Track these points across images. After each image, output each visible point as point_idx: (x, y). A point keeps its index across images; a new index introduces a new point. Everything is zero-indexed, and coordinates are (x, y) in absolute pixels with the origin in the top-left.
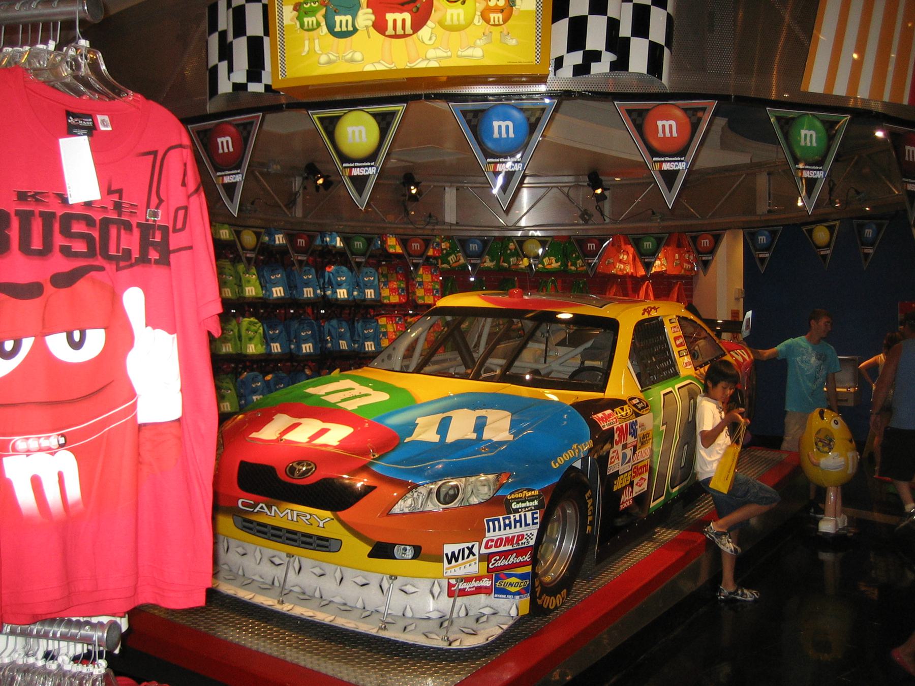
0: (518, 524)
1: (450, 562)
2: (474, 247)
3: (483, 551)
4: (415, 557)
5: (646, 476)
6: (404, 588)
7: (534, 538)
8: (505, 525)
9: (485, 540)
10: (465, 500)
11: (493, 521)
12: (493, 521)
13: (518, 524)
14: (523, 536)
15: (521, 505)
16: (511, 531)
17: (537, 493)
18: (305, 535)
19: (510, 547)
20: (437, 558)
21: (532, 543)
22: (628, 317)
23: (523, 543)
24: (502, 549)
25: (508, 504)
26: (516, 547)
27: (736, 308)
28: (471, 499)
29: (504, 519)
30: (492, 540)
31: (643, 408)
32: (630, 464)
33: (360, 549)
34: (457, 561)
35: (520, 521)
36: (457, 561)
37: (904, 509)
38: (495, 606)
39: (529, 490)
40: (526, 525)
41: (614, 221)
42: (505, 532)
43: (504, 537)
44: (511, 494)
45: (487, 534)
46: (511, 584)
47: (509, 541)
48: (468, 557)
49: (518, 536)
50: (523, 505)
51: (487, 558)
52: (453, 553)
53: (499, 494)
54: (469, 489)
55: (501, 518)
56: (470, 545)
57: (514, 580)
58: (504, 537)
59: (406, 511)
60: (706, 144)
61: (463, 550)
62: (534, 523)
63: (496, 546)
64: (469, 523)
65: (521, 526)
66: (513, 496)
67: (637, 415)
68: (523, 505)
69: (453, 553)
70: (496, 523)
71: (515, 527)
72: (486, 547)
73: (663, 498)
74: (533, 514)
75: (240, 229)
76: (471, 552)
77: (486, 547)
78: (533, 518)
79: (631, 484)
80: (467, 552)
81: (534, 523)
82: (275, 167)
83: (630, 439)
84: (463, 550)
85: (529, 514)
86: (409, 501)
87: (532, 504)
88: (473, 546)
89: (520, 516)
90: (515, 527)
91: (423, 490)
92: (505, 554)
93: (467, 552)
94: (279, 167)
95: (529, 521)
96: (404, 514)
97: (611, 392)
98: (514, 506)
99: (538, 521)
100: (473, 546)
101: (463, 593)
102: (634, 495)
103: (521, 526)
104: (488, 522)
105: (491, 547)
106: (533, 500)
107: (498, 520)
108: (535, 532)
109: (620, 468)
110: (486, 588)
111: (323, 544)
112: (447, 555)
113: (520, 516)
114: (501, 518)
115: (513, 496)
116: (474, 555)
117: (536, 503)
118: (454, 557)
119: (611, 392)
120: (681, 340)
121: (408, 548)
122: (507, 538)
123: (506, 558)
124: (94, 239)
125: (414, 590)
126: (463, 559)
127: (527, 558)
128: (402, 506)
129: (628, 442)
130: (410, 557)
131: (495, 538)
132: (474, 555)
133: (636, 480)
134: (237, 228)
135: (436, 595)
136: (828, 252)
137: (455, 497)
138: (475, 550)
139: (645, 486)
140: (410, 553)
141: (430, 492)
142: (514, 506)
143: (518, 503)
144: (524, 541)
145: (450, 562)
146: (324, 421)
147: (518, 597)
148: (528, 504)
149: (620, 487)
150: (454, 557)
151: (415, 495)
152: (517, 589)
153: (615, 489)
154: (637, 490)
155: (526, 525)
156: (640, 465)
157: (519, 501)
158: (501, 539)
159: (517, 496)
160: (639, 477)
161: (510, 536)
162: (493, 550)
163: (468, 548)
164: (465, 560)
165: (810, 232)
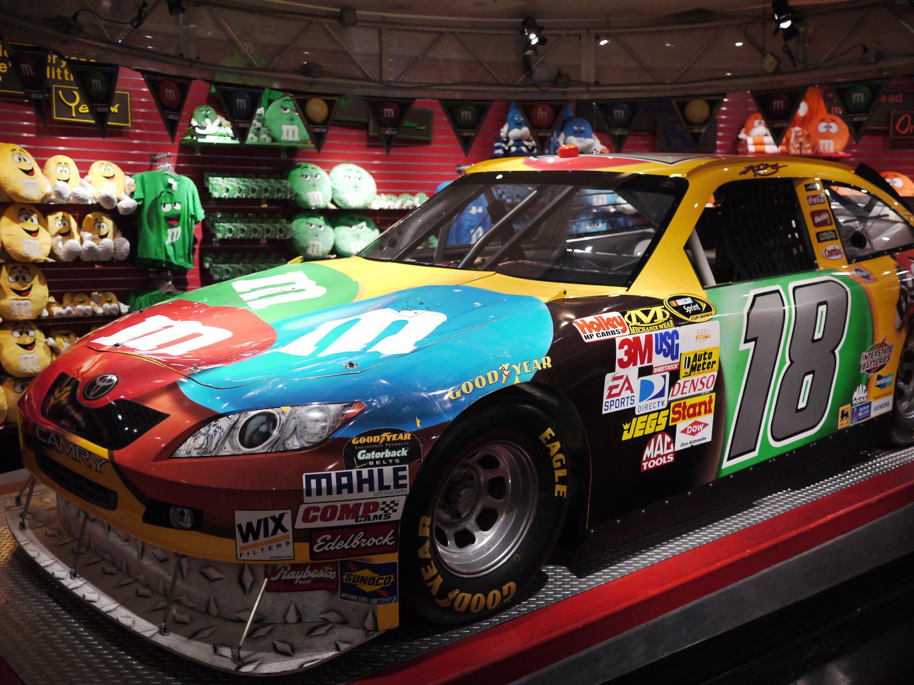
0: (366, 486)
1: (245, 539)
2: (619, 113)
3: (300, 524)
5: (709, 419)
6: (205, 571)
9: (302, 508)
11: (318, 479)
12: (318, 479)
13: (366, 486)
14: (376, 505)
16: (351, 496)
17: (408, 436)
19: (351, 522)
21: (396, 516)
24: (335, 523)
28: (289, 442)
29: (339, 477)
30: (316, 509)
32: (665, 399)
35: (370, 480)
36: (256, 537)
37: (417, 554)
39: (393, 431)
42: (340, 497)
43: (339, 505)
44: (359, 437)
45: (306, 499)
46: (364, 580)
47: (348, 511)
49: (367, 505)
50: (379, 455)
52: (250, 525)
53: (339, 435)
56: (277, 513)
57: (366, 573)
58: (339, 505)
59: (194, 454)
62: (397, 486)
63: (324, 518)
65: (371, 489)
66: (363, 440)
67: (677, 322)
68: (379, 455)
69: (250, 525)
71: (360, 490)
73: (754, 454)
74: (396, 471)
77: (305, 519)
78: (397, 478)
79: (670, 431)
80: (272, 525)
81: (397, 486)
83: (659, 360)
84: (266, 520)
85: (388, 471)
86: (201, 440)
87: (394, 454)
92: (345, 532)
98: (361, 455)
99: (407, 482)
100: (282, 516)
101: (288, 586)
102: (678, 447)
104: (309, 479)
105: (315, 519)
106: (397, 448)
107: (328, 477)
108: (402, 501)
110: (328, 581)
112: (240, 526)
115: (363, 440)
116: (284, 530)
118: (251, 532)
121: (186, 512)
122: (345, 508)
124: (71, 102)
125: (219, 575)
126: (266, 535)
131: (322, 506)
132: (284, 530)
133: (681, 425)
134: (300, 97)
138: (287, 522)
139: (706, 435)
140: (188, 522)
141: (233, 427)
142: (361, 455)
143: (369, 451)
144: (379, 513)
145: (245, 539)
148: (388, 454)
149: (638, 434)
150: (251, 532)
151: (213, 429)
153: (626, 436)
154: (683, 441)
155: (382, 487)
156: (689, 402)
157: (369, 448)
158: (334, 508)
159: (369, 439)
160: (688, 422)
161: (351, 504)
162: (319, 524)
163: (273, 518)
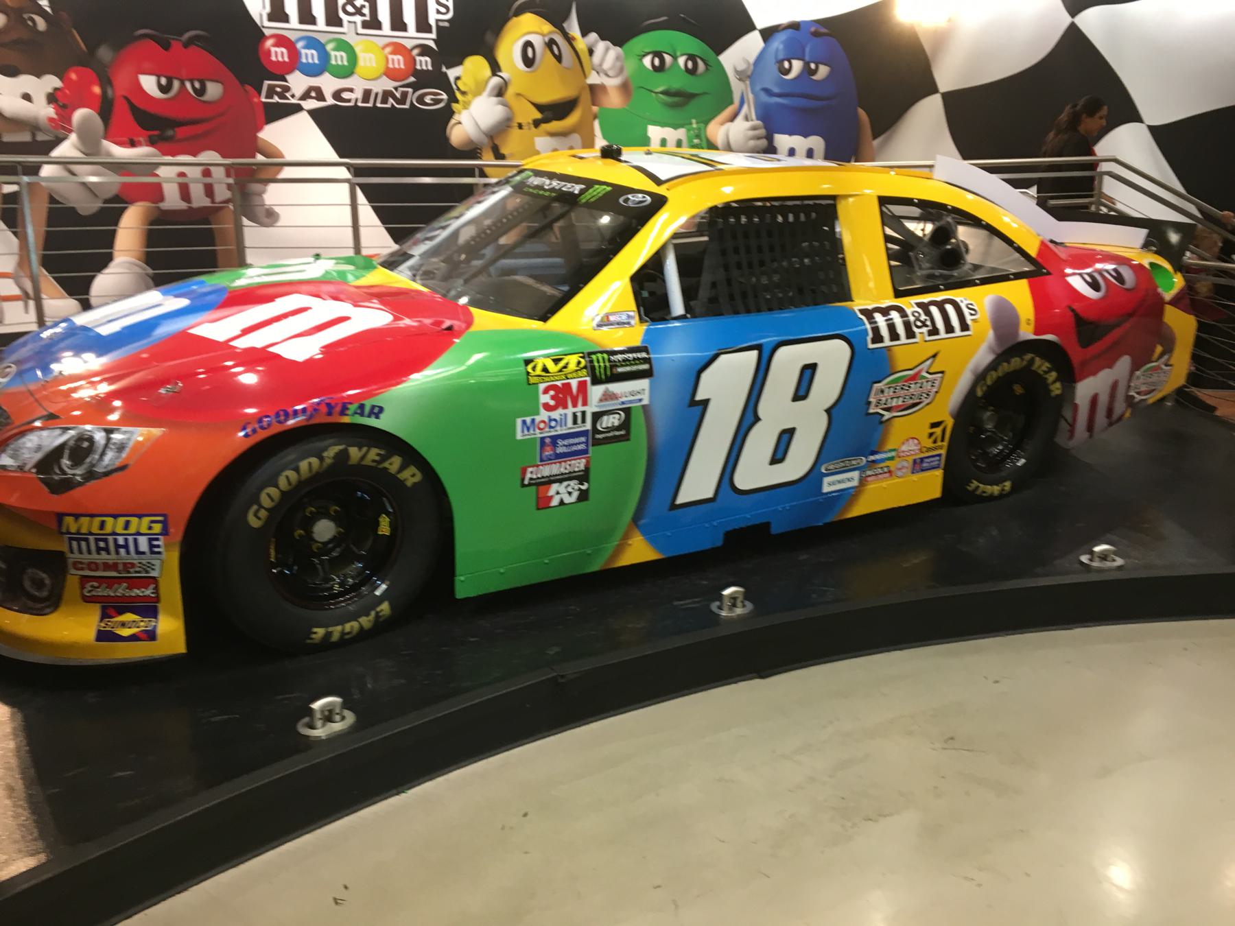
8: (118, 546)
46: (123, 625)
74: (150, 540)
78: (151, 546)
89: (126, 540)
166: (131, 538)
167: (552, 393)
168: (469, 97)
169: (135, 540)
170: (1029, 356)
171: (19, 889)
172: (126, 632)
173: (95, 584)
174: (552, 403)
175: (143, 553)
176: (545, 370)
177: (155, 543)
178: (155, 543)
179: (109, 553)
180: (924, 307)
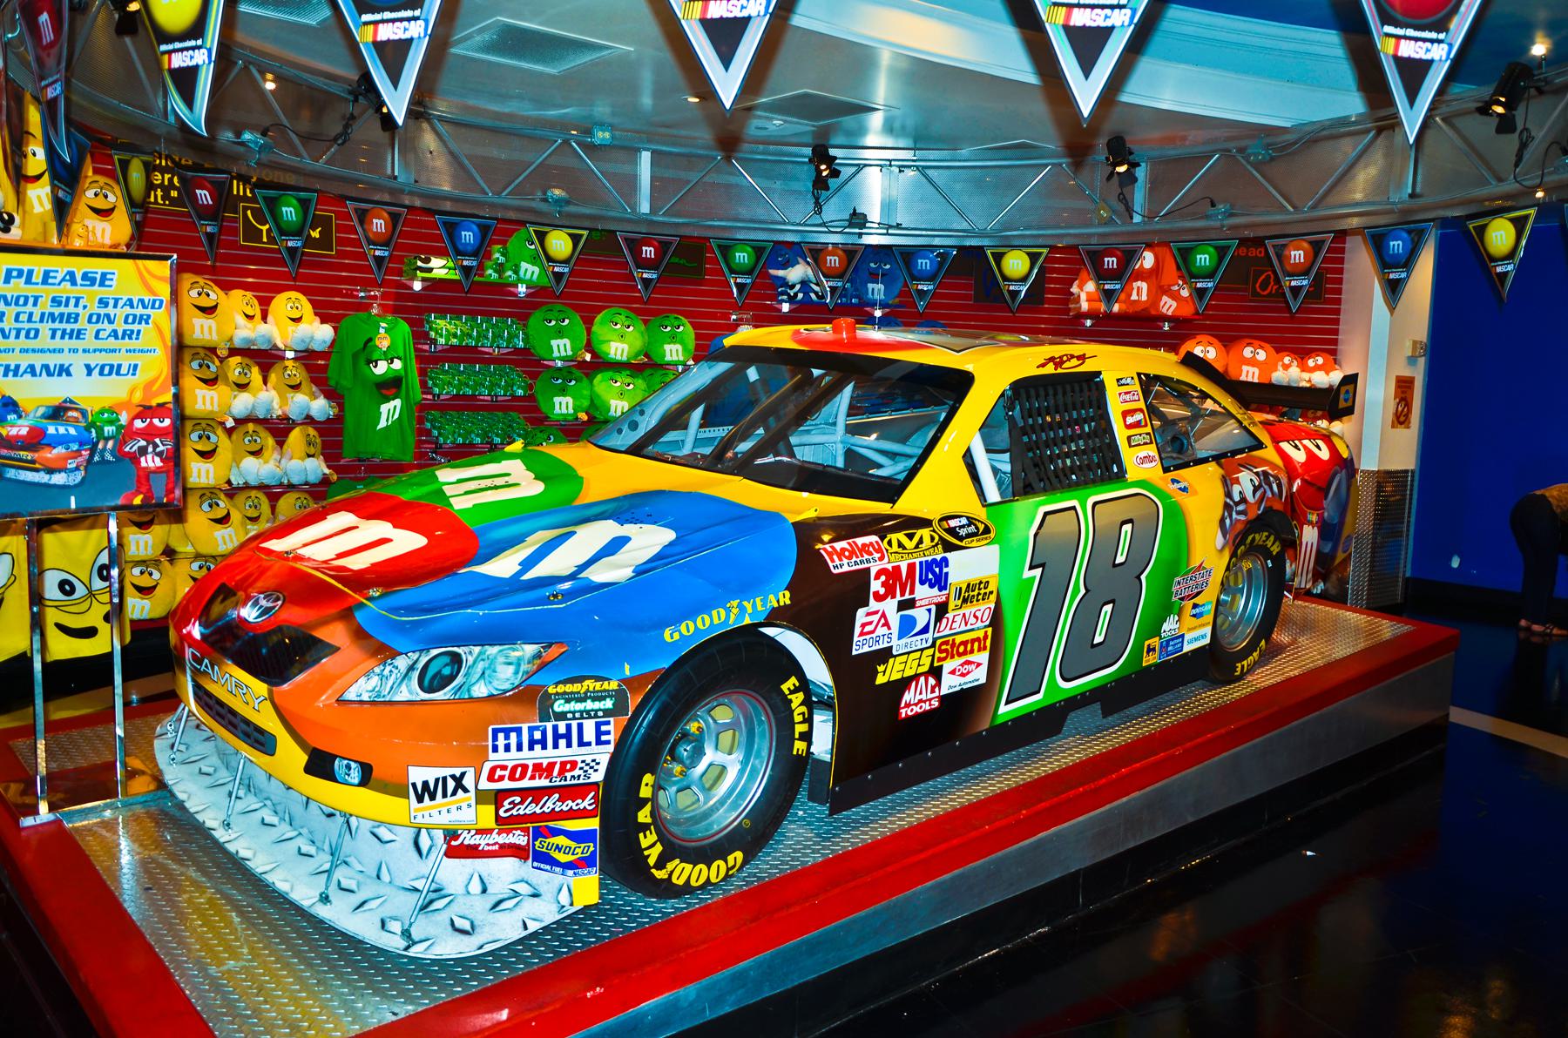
0: (562, 742)
1: (420, 799)
3: (485, 784)
4: (364, 782)
7: (603, 769)
8: (557, 737)
10: (465, 688)
11: (507, 732)
12: (507, 732)
13: (562, 742)
14: (574, 764)
15: (574, 706)
17: (614, 685)
18: (247, 722)
20: (398, 788)
22: (997, 367)
23: (572, 778)
25: (548, 700)
26: (557, 782)
27: (1406, 373)
29: (531, 730)
30: (504, 768)
31: (969, 535)
32: (929, 636)
33: (290, 756)
34: (433, 798)
35: (568, 736)
36: (433, 798)
38: (534, 882)
40: (581, 743)
41: (1150, 216)
43: (530, 763)
44: (557, 684)
45: (492, 756)
46: (558, 848)
48: (454, 793)
49: (563, 764)
50: (580, 706)
51: (499, 797)
52: (425, 784)
53: (534, 681)
54: (480, 666)
55: (525, 727)
56: (457, 772)
57: (561, 840)
58: (530, 763)
59: (365, 698)
60: (1157, 41)
61: (445, 779)
62: (599, 742)
63: (512, 778)
64: (468, 729)
65: (569, 745)
66: (561, 689)
67: (949, 547)
68: (580, 706)
69: (425, 784)
70: (513, 735)
71: (556, 746)
72: (491, 778)
74: (598, 725)
75: (546, 229)
76: (459, 781)
77: (491, 778)
78: (599, 733)
80: (451, 784)
82: (600, 134)
83: (923, 592)
84: (445, 779)
86: (375, 680)
87: (597, 705)
88: (463, 774)
89: (569, 727)
90: (556, 746)
91: (402, 663)
93: (451, 784)
94: (607, 135)
95: (589, 735)
96: (361, 702)
97: (907, 504)
99: (611, 737)
100: (463, 774)
101: (472, 852)
102: (945, 691)
103: (569, 745)
104: (495, 732)
105: (501, 778)
107: (519, 731)
109: (895, 642)
111: (262, 741)
112: (414, 785)
113: (569, 727)
114: (525, 727)
115: (561, 689)
116: (466, 790)
117: (608, 704)
118: (426, 792)
119: (907, 504)
120: (1139, 416)
121: (353, 765)
123: (536, 801)
126: (445, 795)
127: (586, 803)
128: (362, 689)
129: (917, 595)
130: (356, 781)
131: (510, 764)
132: (466, 790)
133: (948, 665)
135: (424, 852)
136: (1510, 268)
137: (446, 681)
138: (468, 781)
139: (980, 676)
140: (355, 776)
142: (559, 706)
143: (568, 701)
144: (577, 772)
145: (420, 799)
146: (621, 522)
147: (570, 872)
148: (589, 705)
149: (896, 676)
150: (426, 792)
152: (570, 858)
153: (880, 680)
156: (959, 639)
158: (525, 767)
162: (506, 784)
163: (453, 777)
164: (449, 799)
165: (1482, 230)
166: (574, 724)
167: (883, 578)
168: (423, 179)
169: (580, 727)
170: (660, 874)
171: (1143, 706)
172: (562, 858)
173: (518, 799)
174: (882, 591)
175: (589, 744)
176: (900, 545)
177: (604, 728)
178: (604, 728)
179: (544, 747)
180: (862, 634)
